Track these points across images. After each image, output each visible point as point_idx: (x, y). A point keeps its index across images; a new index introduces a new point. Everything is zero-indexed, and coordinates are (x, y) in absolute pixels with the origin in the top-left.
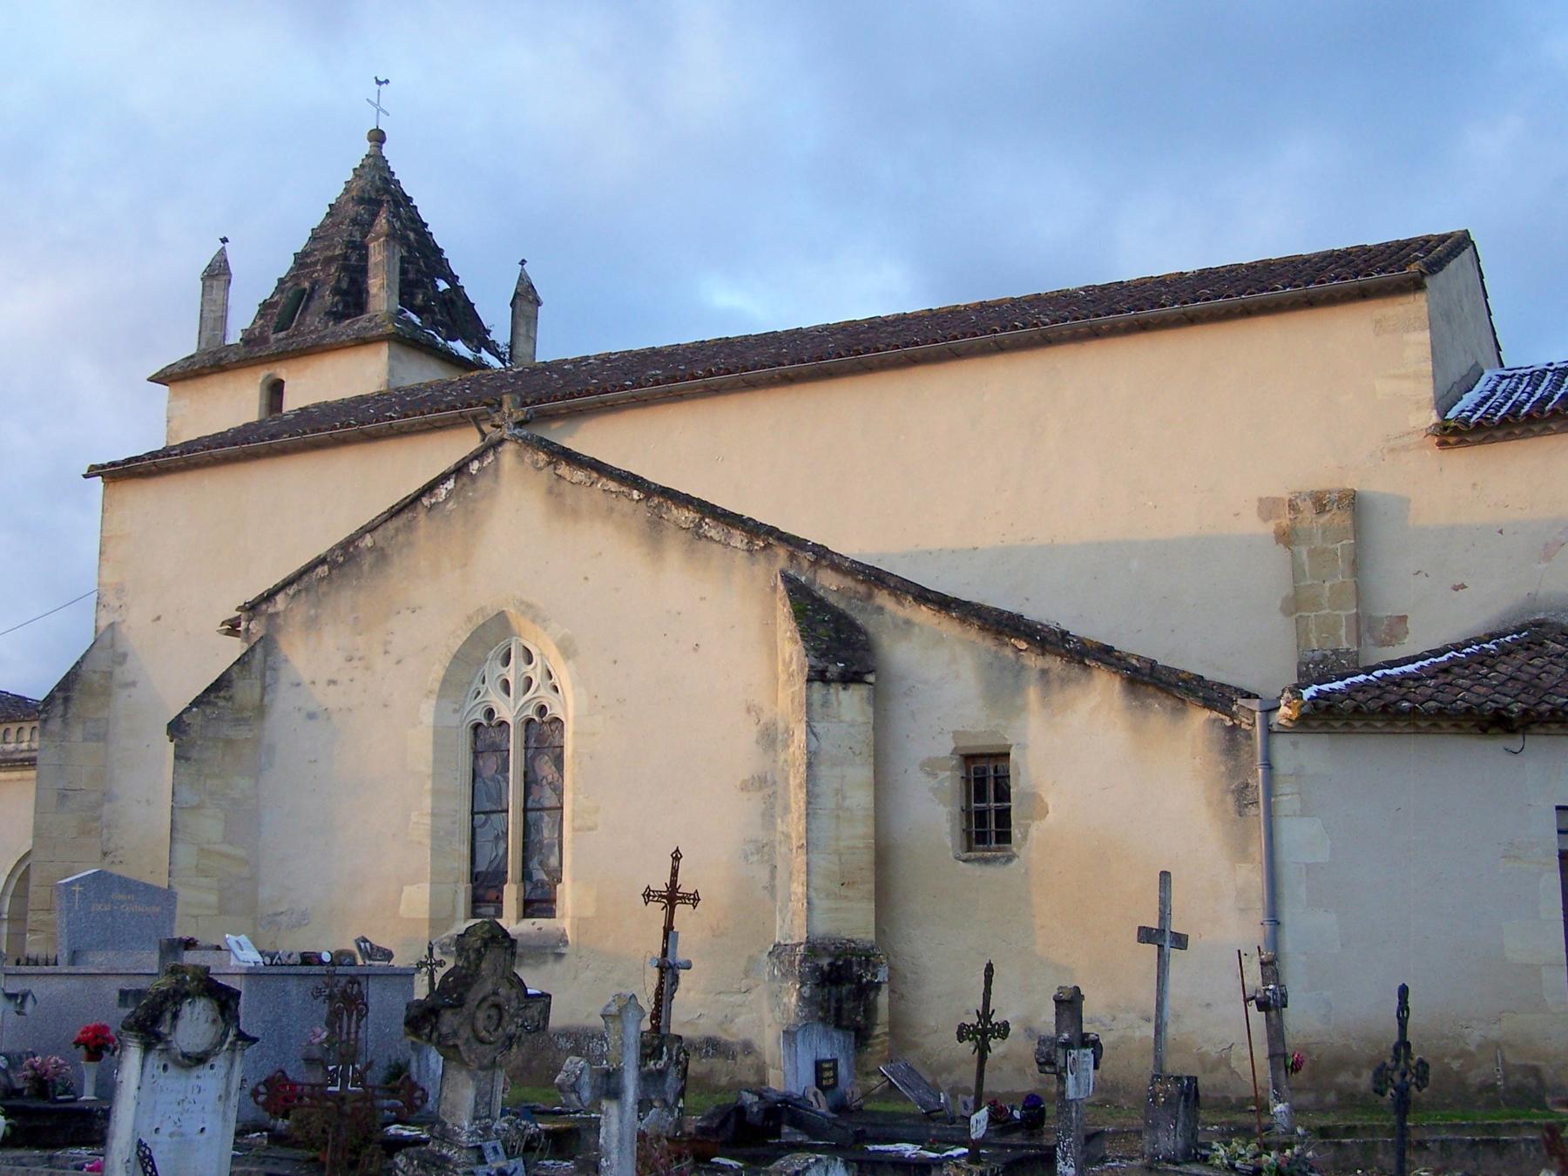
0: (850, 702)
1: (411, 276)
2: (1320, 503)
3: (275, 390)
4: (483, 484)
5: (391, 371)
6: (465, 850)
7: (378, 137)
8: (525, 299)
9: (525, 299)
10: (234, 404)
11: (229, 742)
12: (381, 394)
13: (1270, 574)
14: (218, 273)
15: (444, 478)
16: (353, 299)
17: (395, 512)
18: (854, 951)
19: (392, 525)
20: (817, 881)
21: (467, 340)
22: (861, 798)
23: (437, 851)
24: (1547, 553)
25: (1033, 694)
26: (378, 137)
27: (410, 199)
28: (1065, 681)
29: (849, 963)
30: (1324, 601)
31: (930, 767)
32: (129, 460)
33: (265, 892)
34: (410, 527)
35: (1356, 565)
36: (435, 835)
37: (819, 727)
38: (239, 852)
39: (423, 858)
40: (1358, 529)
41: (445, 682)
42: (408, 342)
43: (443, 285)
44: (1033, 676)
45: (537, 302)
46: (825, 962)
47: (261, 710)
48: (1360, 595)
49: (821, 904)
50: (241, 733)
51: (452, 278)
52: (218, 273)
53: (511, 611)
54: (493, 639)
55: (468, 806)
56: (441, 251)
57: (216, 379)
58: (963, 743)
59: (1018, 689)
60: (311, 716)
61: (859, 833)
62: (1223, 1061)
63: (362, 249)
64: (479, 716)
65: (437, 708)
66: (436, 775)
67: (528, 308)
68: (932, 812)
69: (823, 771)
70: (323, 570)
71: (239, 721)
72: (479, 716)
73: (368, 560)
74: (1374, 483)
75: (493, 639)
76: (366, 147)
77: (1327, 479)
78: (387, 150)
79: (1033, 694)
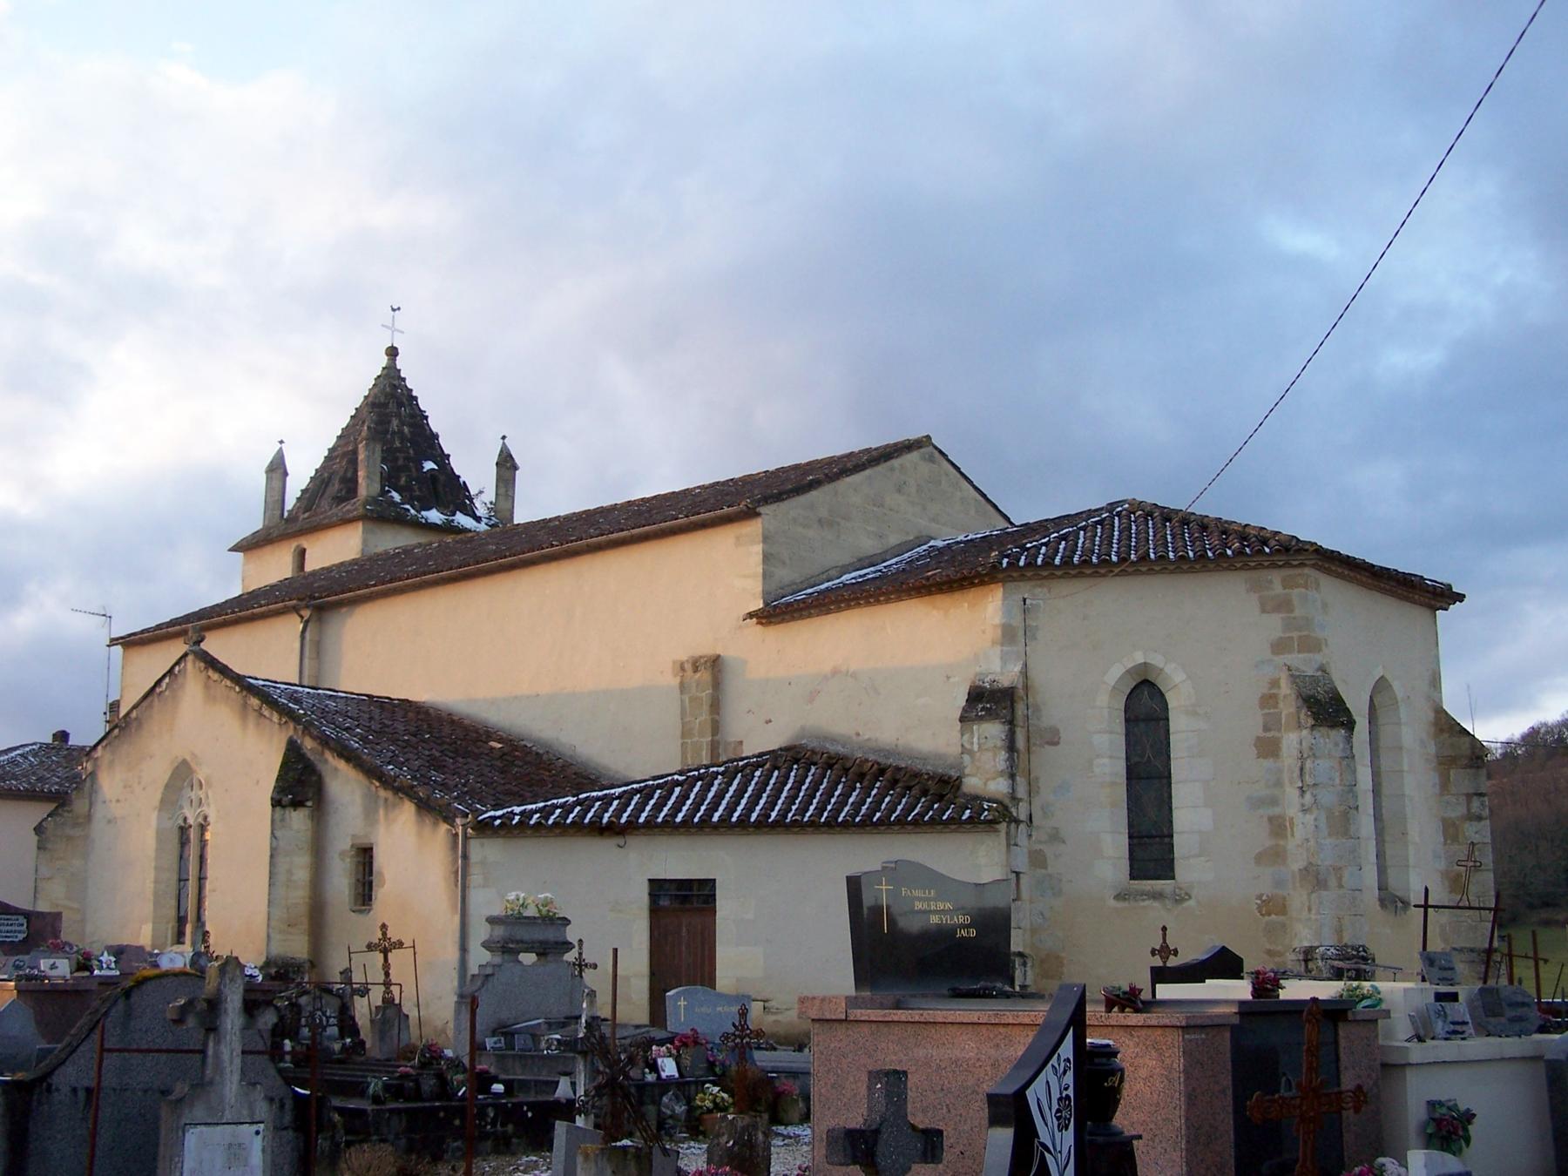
0: (299, 820)
1: (400, 462)
2: (696, 665)
3: (301, 554)
4: (180, 680)
5: (365, 542)
6: (174, 903)
7: (393, 352)
8: (506, 465)
9: (506, 465)
10: (276, 567)
11: (70, 838)
12: (354, 562)
13: (668, 716)
14: (278, 469)
15: (164, 676)
16: (350, 487)
17: (145, 697)
18: (292, 965)
19: (144, 704)
20: (273, 923)
21: (441, 507)
22: (302, 875)
23: (156, 904)
24: (812, 696)
25: (382, 812)
26: (393, 352)
27: (416, 398)
28: (394, 806)
29: (287, 972)
30: (695, 732)
31: (342, 854)
32: (142, 632)
33: (89, 928)
34: (151, 706)
35: (716, 705)
36: (156, 894)
37: (278, 834)
38: (75, 905)
39: (148, 908)
40: (717, 684)
41: (162, 801)
42: (381, 515)
43: (429, 465)
44: (381, 802)
45: (515, 468)
46: (273, 971)
47: (89, 817)
48: (716, 727)
49: (276, 936)
50: (77, 832)
51: (442, 459)
52: (278, 469)
53: (188, 758)
54: (182, 776)
55: (175, 877)
56: (436, 436)
57: (268, 549)
58: (358, 841)
59: (376, 811)
60: (109, 822)
61: (299, 895)
62: (444, 1031)
63: (355, 452)
64: (181, 822)
65: (159, 818)
66: (157, 858)
67: (508, 474)
68: (340, 881)
69: (280, 859)
70: (116, 731)
71: (76, 825)
72: (181, 822)
73: (135, 724)
74: (729, 651)
75: (182, 776)
76: (384, 361)
77: (706, 649)
78: (400, 363)
79: (382, 812)
